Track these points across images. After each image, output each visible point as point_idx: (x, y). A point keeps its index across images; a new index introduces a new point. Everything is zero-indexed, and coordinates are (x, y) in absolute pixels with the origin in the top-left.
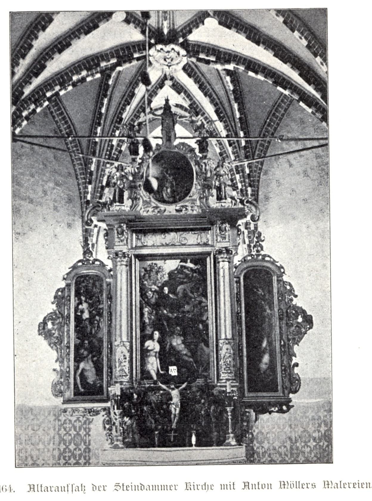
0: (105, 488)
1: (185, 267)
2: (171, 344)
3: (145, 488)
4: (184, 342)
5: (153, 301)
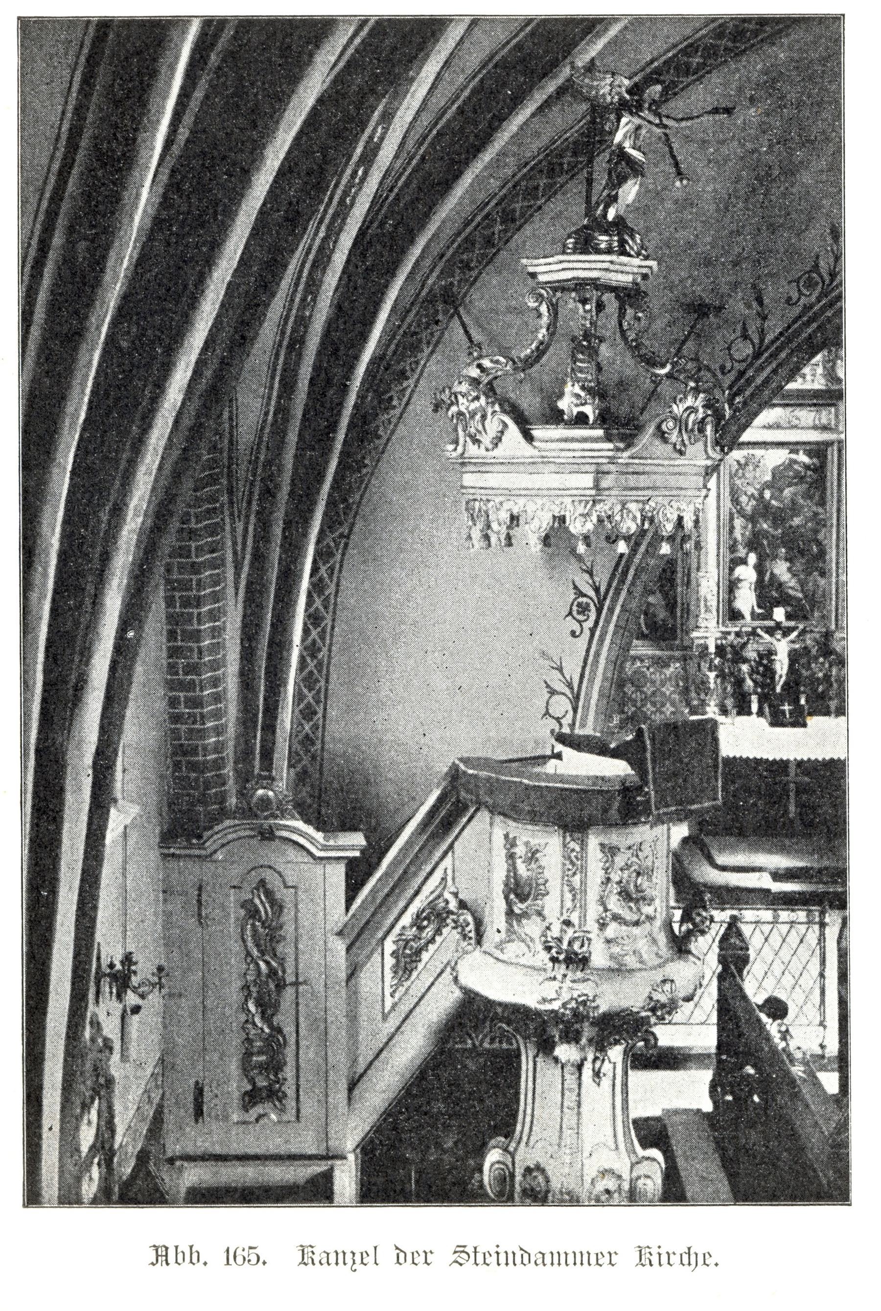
0: (430, 1258)
1: (795, 462)
2: (772, 573)
3: (533, 1259)
4: (789, 570)
5: (749, 509)
